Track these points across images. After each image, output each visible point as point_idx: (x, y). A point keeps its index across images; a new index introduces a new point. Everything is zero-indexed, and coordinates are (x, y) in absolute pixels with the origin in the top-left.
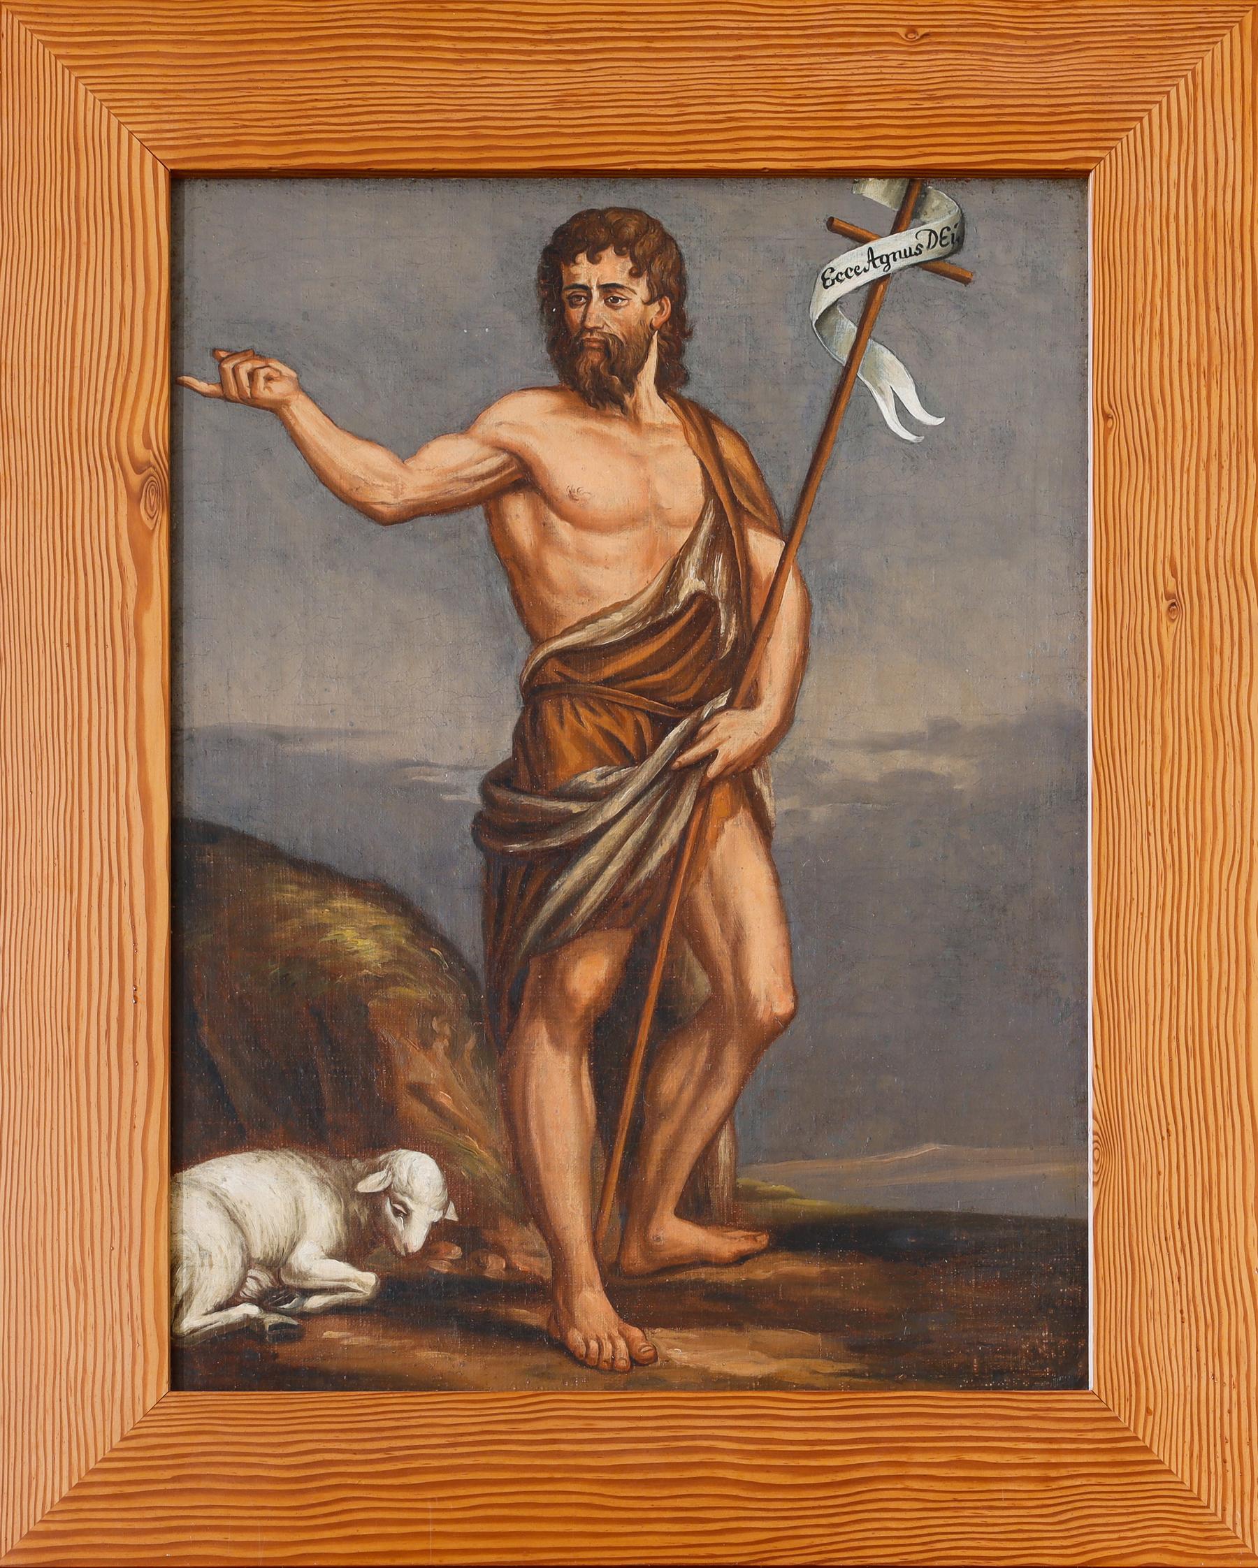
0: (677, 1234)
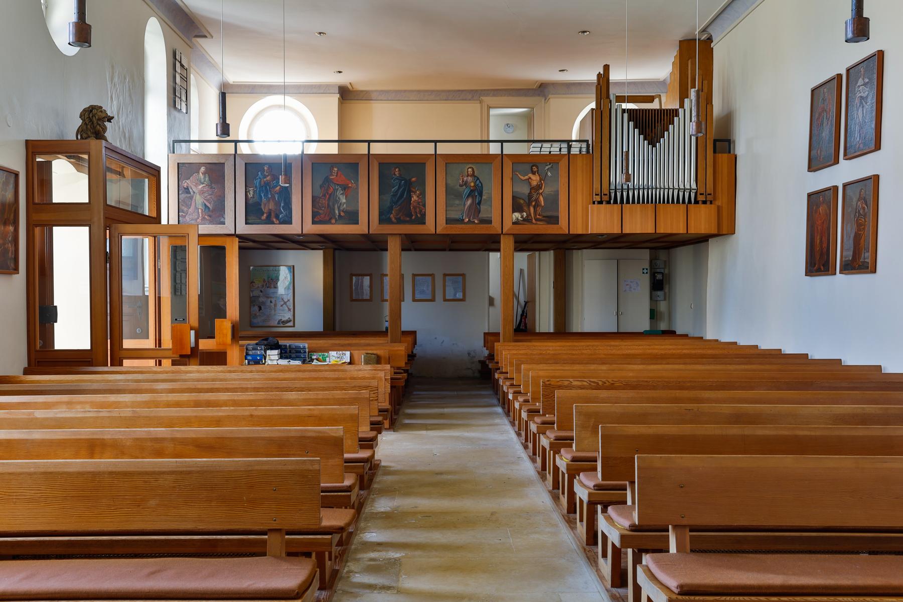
0: (86, 157)
